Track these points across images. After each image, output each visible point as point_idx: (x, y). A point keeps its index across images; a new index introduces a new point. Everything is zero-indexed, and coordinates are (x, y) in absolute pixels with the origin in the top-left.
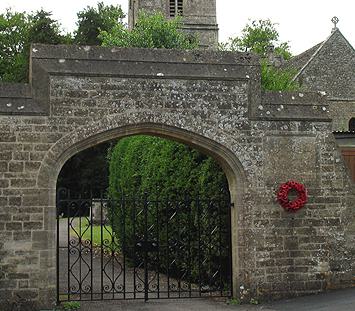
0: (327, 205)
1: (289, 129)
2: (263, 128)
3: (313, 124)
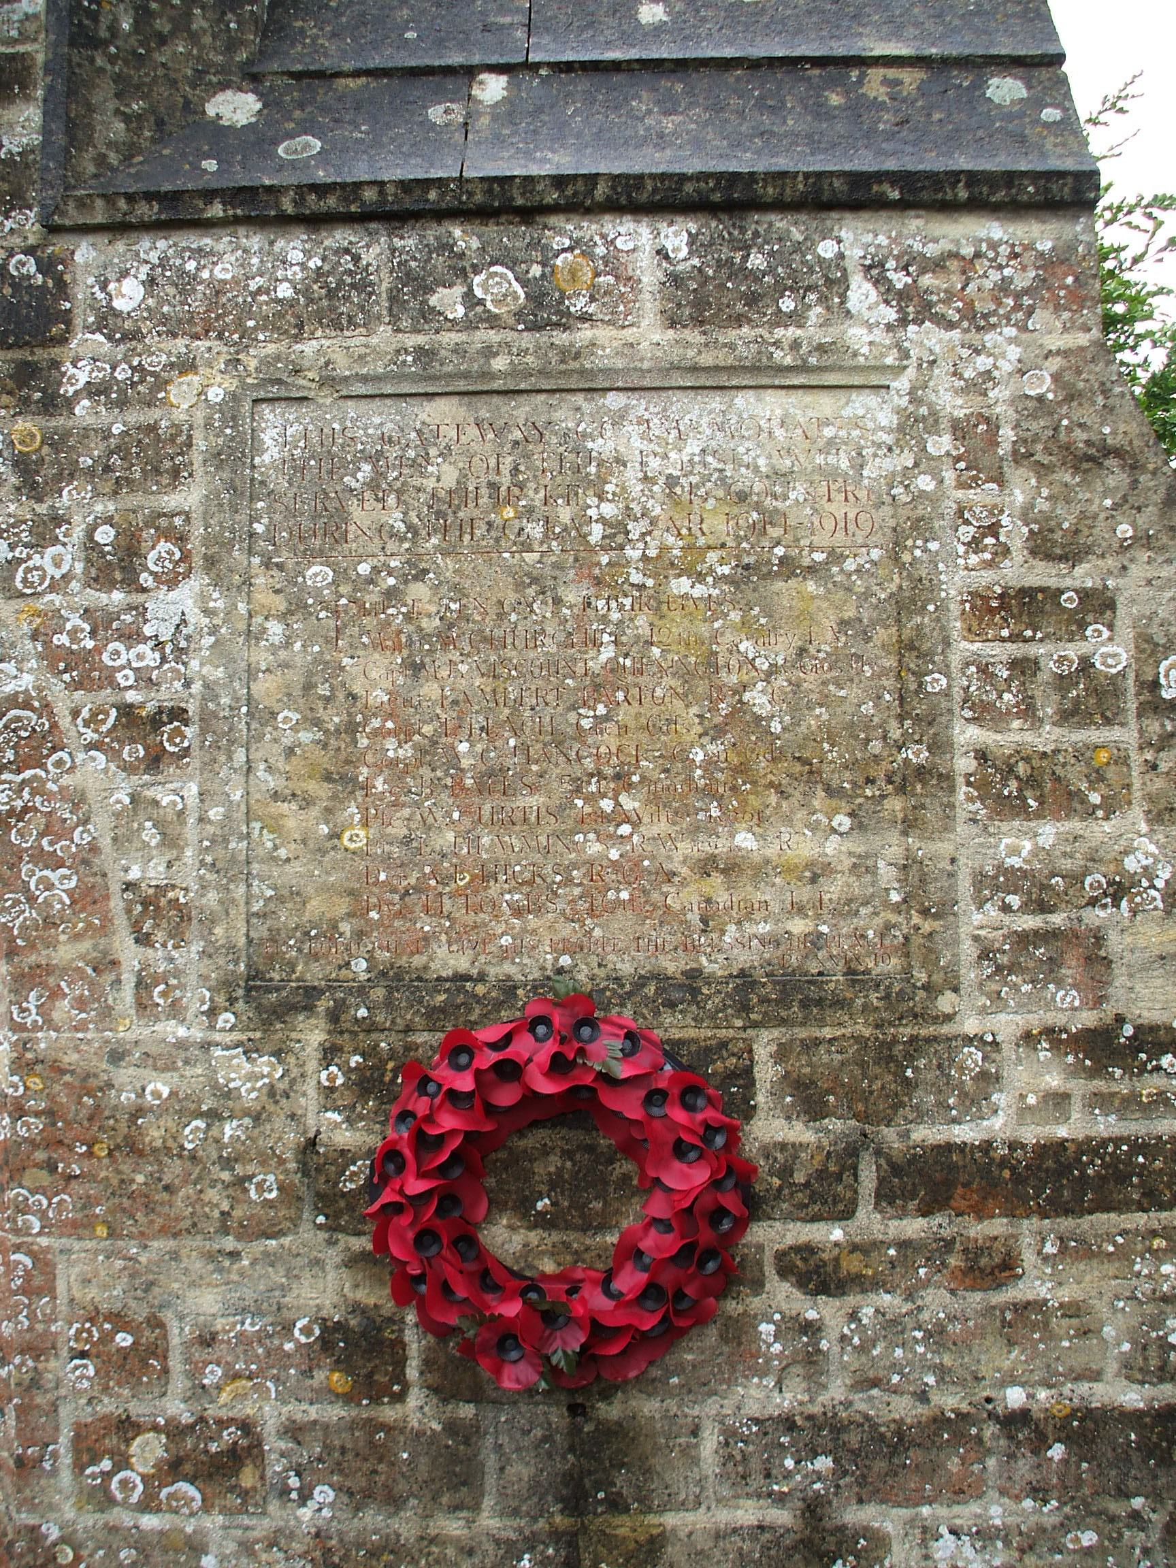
0: (1032, 1238)
1: (544, 309)
2: (221, 318)
3: (851, 240)
